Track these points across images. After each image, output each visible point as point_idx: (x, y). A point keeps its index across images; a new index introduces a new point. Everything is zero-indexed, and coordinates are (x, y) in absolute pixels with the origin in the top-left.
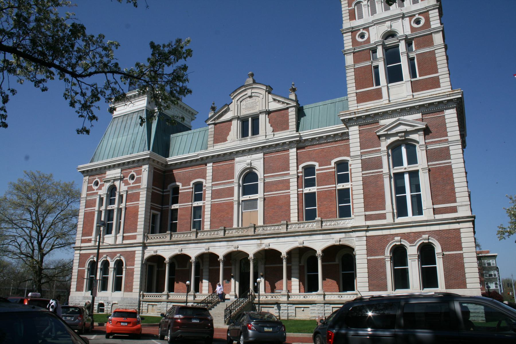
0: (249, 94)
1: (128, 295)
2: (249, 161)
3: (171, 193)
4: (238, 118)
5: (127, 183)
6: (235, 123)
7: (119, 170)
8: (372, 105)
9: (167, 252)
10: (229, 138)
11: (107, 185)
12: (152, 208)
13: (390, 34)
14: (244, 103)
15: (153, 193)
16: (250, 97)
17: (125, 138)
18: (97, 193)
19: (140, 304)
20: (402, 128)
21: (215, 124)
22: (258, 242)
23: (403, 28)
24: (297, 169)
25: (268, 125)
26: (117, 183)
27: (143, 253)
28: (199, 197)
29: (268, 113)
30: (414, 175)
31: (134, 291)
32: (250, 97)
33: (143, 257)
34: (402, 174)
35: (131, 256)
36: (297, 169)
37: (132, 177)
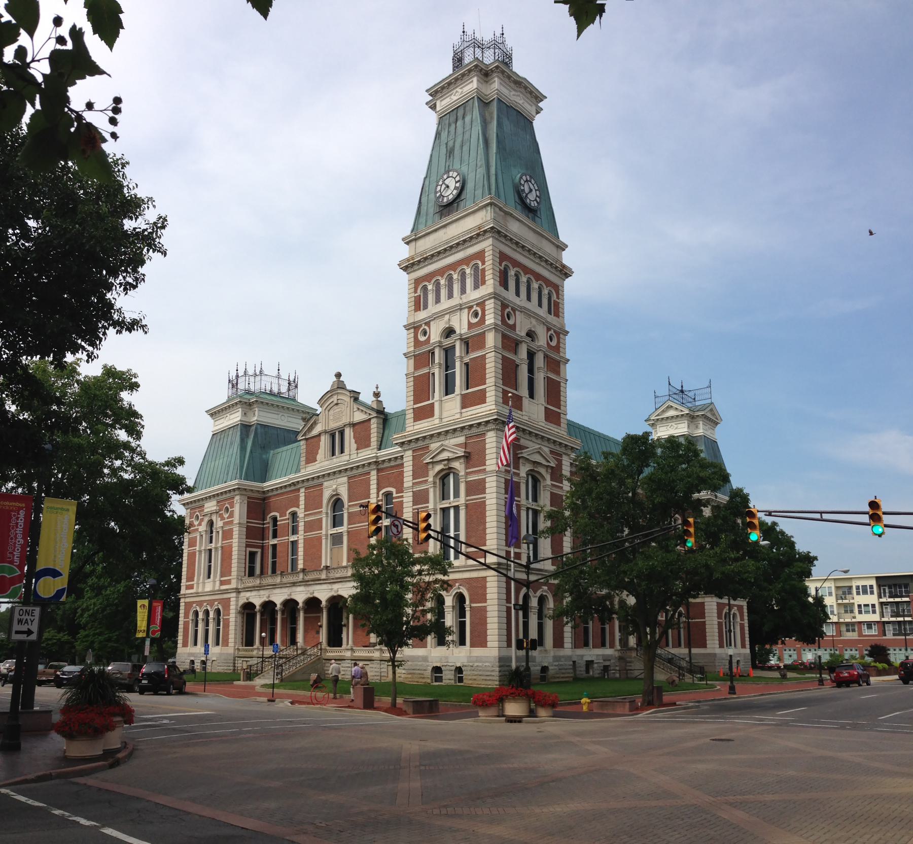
0: (335, 402)
1: (478, 652)
2: (334, 487)
3: (271, 526)
4: (326, 432)
5: (222, 518)
6: (323, 438)
7: (214, 503)
8: (426, 424)
9: (257, 599)
10: (319, 457)
11: (206, 519)
12: (247, 546)
13: (449, 332)
14: (331, 412)
15: (248, 528)
16: (337, 404)
17: (221, 461)
18: (197, 530)
19: (234, 660)
20: (445, 455)
21: (306, 439)
22: (330, 586)
23: (461, 324)
24: (378, 496)
25: (353, 441)
26: (214, 518)
27: (237, 601)
28: (295, 531)
29: (353, 425)
30: (457, 508)
31: (489, 644)
32: (337, 404)
33: (237, 605)
34: (448, 508)
35: (226, 603)
36: (378, 496)
37: (227, 509)
